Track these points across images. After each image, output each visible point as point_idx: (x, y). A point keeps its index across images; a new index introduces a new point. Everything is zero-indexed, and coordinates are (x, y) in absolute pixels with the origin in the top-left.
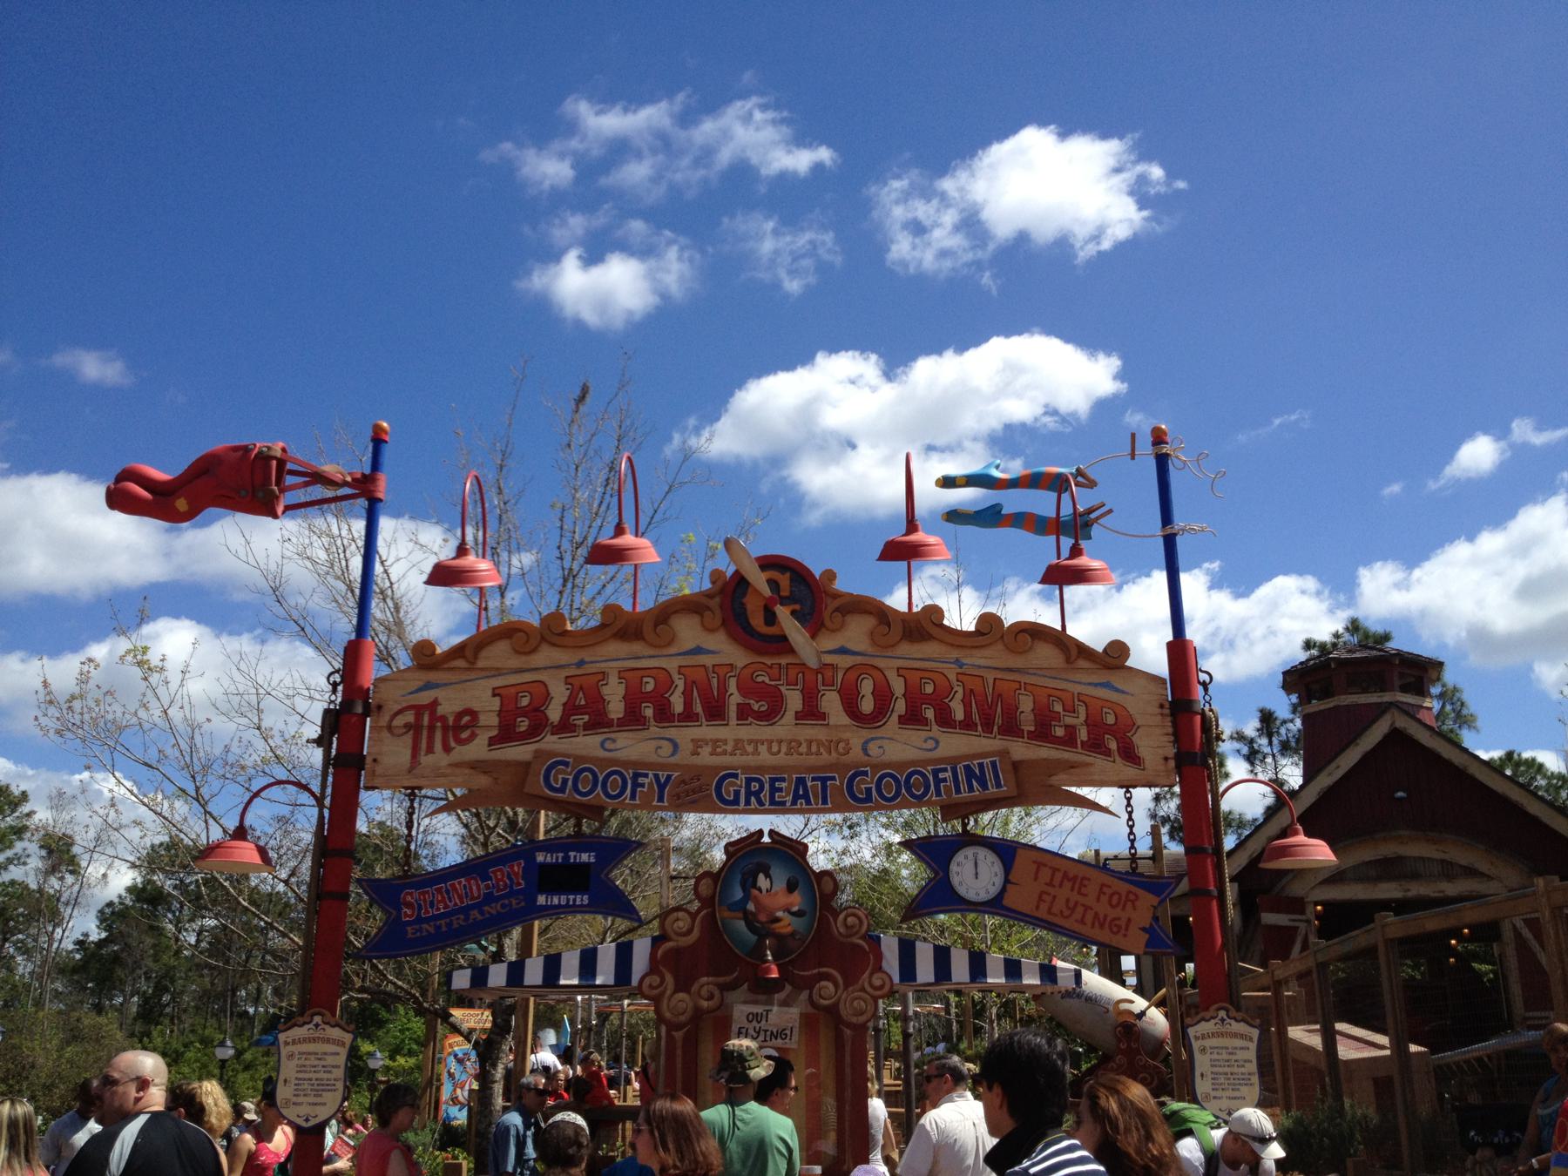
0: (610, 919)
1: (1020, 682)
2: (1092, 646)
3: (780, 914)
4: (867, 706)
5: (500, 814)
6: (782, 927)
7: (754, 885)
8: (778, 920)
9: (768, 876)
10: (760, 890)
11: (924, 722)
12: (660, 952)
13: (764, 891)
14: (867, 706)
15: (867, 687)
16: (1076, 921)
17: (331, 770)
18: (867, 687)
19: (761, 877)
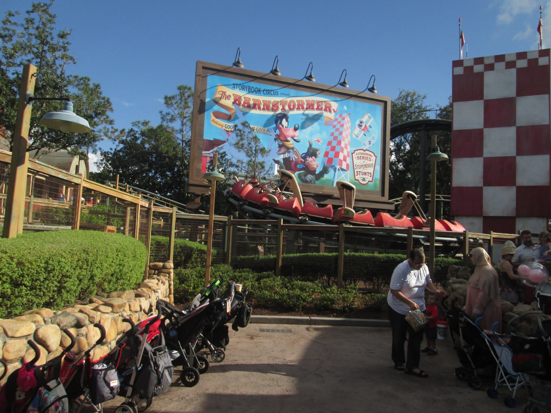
0: (97, 367)
1: (385, 103)
2: (484, 82)
3: (289, 139)
4: (292, 107)
5: (206, 297)
6: (290, 144)
7: (281, 123)
8: (287, 141)
9: (287, 121)
10: (283, 126)
11: (327, 111)
12: (32, 131)
13: (284, 127)
14: (292, 107)
15: (292, 104)
16: (365, 146)
17: (446, 221)
18: (292, 104)
19: (284, 120)
